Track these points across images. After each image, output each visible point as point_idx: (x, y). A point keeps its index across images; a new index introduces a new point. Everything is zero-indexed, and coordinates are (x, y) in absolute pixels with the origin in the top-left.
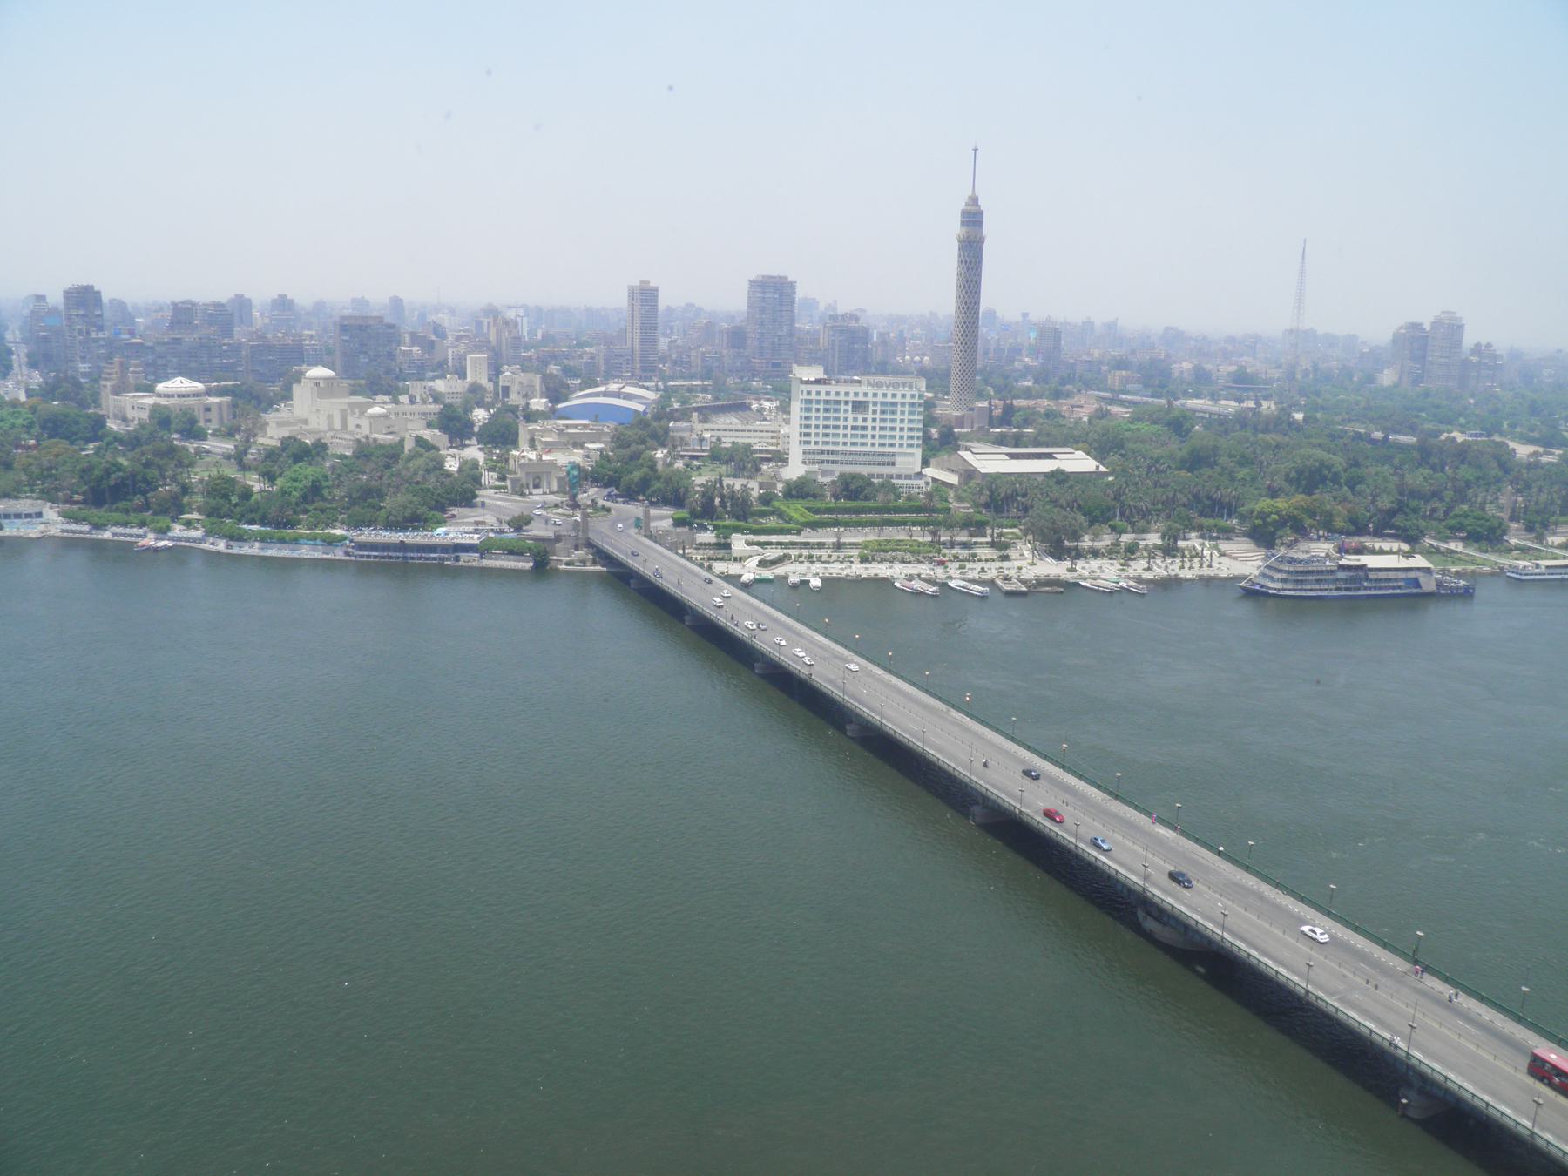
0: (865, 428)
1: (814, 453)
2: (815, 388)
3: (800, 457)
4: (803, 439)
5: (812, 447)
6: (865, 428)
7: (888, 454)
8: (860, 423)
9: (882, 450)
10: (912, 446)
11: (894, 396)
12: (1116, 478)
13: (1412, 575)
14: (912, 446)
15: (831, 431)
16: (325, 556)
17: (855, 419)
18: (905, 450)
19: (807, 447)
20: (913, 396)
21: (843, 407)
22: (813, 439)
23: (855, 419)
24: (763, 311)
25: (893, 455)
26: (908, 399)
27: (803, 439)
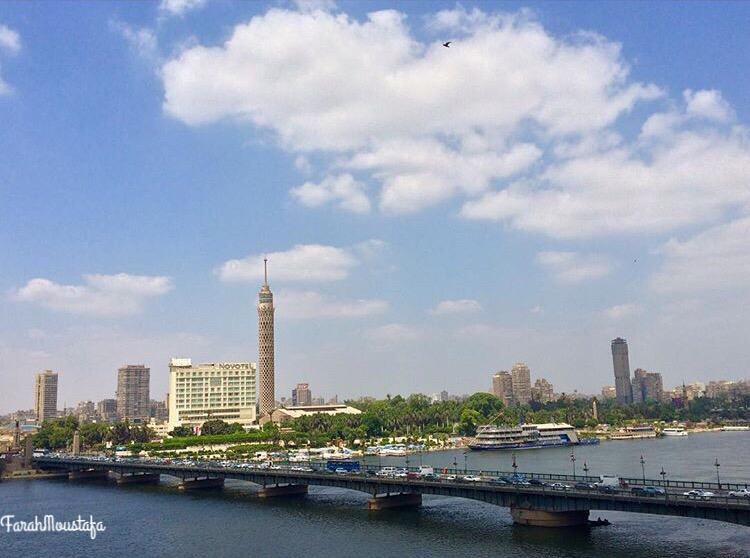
0: (237, 378)
1: (186, 412)
2: (185, 371)
3: (178, 416)
4: (179, 404)
5: (185, 409)
6: (237, 378)
7: (236, 411)
8: (216, 391)
9: (231, 408)
10: (249, 404)
11: (237, 373)
12: (90, 513)
13: (563, 432)
14: (249, 404)
15: (197, 398)
16: (61, 527)
17: (213, 389)
18: (245, 406)
19: (182, 409)
20: (248, 372)
21: (204, 381)
22: (185, 403)
23: (213, 389)
24: (128, 386)
25: (238, 410)
26: (246, 375)
27: (179, 404)
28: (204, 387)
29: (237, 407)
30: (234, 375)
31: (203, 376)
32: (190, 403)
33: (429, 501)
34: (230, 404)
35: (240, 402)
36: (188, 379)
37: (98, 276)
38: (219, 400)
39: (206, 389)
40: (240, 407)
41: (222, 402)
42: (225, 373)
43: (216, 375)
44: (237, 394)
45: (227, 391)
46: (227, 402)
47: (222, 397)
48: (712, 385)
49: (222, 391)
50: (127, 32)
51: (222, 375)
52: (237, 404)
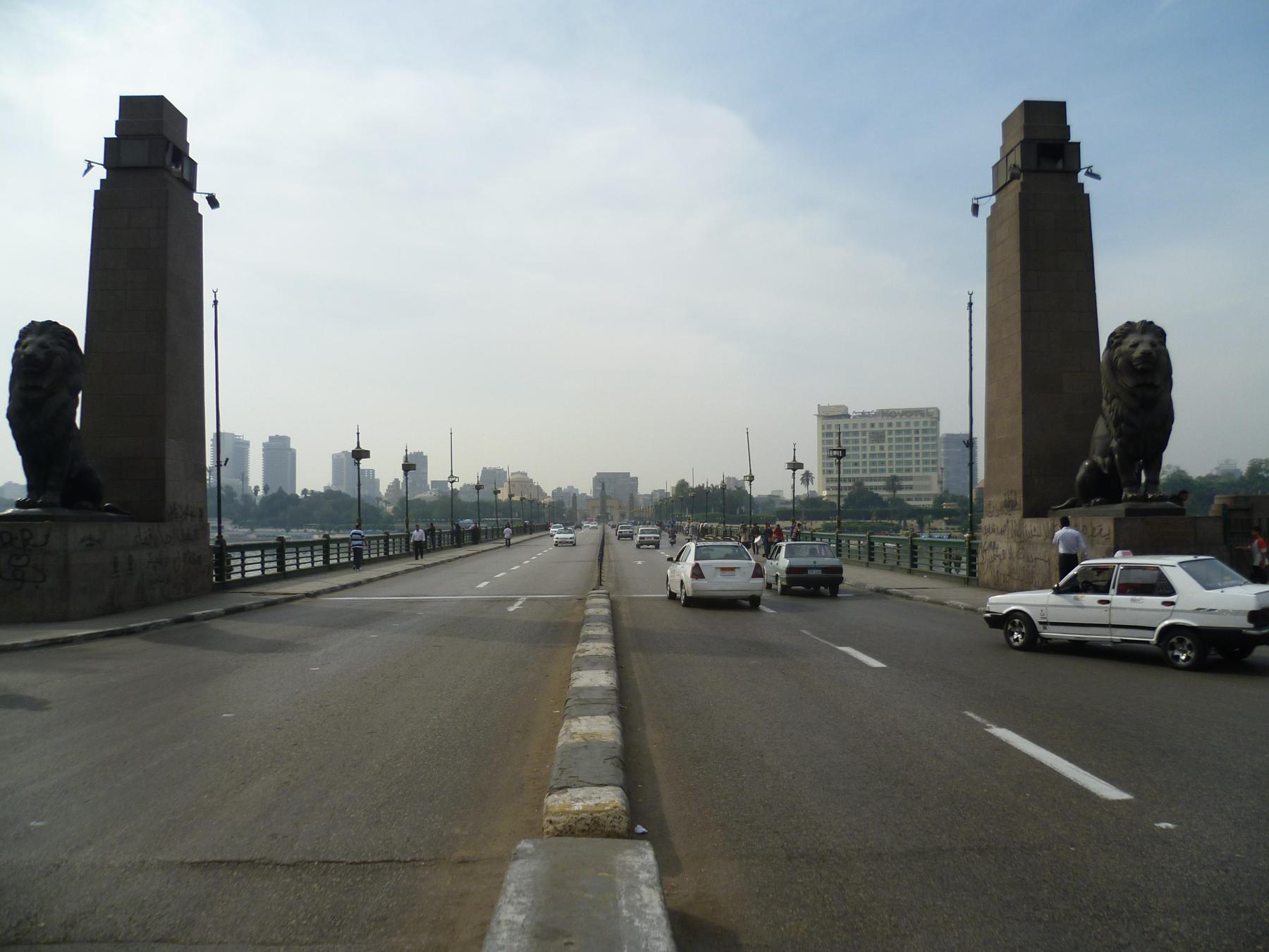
8: (877, 451)
14: (926, 470)
17: (873, 448)
18: (921, 474)
23: (873, 448)
28: (861, 445)
29: (908, 474)
30: (903, 427)
31: (859, 429)
32: (921, 466)
33: (654, 547)
34: (873, 471)
35: (914, 466)
36: (917, 432)
37: (1019, 190)
38: (883, 463)
39: (864, 448)
40: (913, 474)
41: (887, 467)
42: (890, 425)
43: (877, 428)
44: (909, 455)
45: (894, 452)
46: (868, 467)
47: (887, 459)
48: (492, 477)
49: (886, 451)
50: (17, 510)
51: (886, 428)
52: (908, 470)
